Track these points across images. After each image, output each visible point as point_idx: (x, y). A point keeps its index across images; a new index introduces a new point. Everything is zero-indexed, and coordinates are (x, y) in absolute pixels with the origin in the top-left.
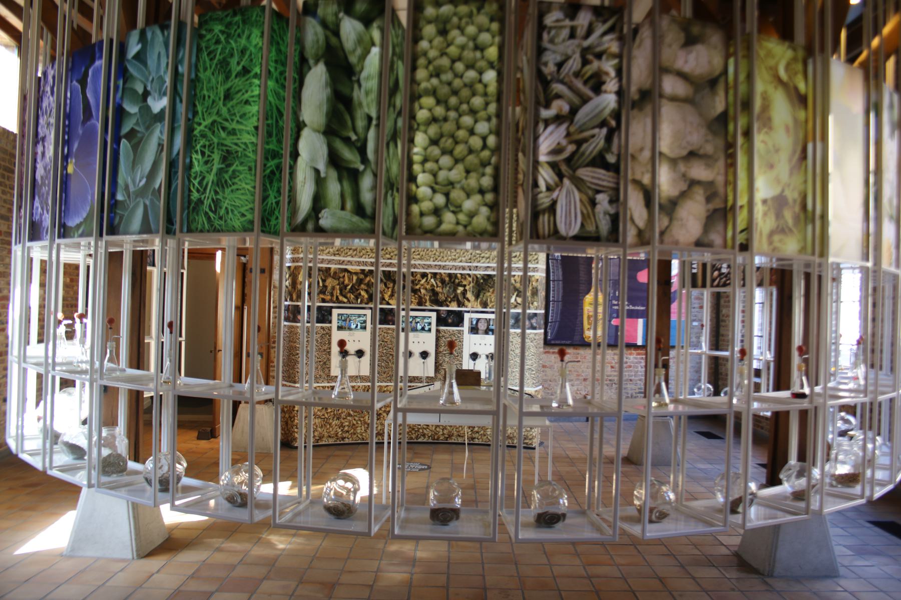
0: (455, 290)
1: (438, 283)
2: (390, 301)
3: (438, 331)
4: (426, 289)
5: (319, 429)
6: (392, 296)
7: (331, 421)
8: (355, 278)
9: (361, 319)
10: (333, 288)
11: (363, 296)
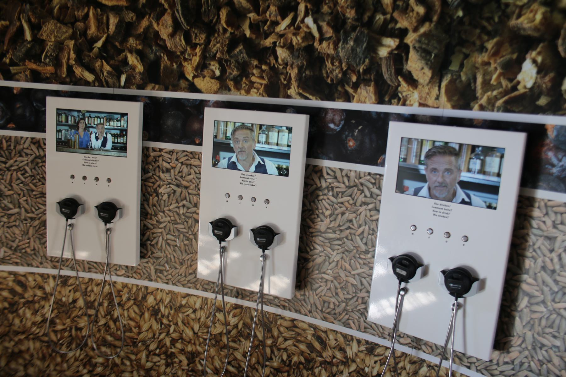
0: (372, 48)
1: (325, 28)
2: (198, 82)
3: (145, 152)
4: (290, 47)
5: (38, 363)
6: (201, 67)
7: (64, 350)
8: (113, 21)
9: (114, 124)
10: (60, 46)
11: (133, 68)
